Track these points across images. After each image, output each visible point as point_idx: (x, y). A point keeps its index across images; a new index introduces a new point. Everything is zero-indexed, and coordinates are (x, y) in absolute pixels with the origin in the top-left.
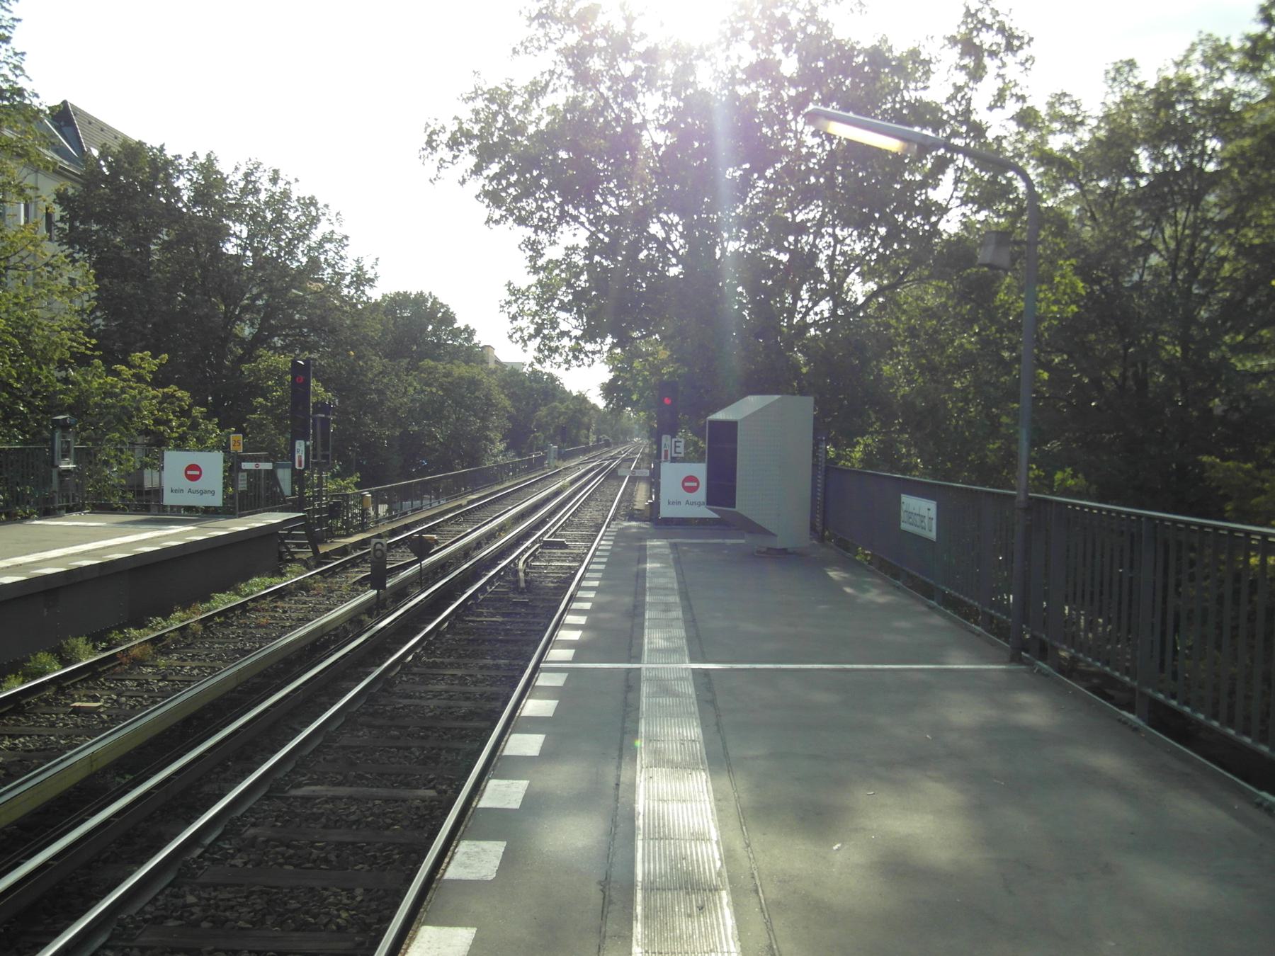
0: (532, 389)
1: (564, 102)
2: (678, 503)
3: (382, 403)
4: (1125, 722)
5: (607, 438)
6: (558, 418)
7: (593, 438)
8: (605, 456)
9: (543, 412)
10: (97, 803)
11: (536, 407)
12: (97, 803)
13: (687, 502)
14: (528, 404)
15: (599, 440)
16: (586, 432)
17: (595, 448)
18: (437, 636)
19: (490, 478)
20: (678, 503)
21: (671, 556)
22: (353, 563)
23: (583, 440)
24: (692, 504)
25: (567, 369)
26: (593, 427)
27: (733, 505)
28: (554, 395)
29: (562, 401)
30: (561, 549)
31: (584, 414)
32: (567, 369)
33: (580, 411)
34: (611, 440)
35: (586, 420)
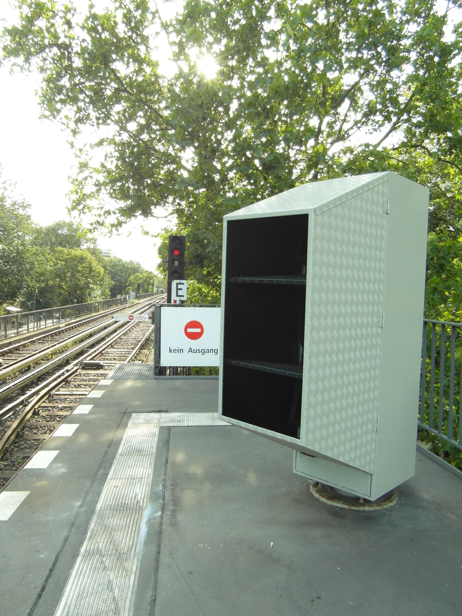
0: (128, 268)
1: (124, 25)
2: (181, 351)
3: (31, 269)
4: (448, 470)
5: (162, 289)
6: (139, 280)
7: (155, 290)
8: (159, 298)
9: (132, 277)
10: (105, 344)
11: (129, 276)
12: (105, 344)
13: (190, 350)
14: (126, 274)
15: (157, 291)
16: (151, 287)
17: (155, 294)
18: (50, 396)
19: (90, 309)
20: (181, 351)
21: (147, 513)
22: (151, 307)
23: (150, 290)
24: (195, 351)
25: (110, 237)
26: (155, 285)
27: (295, 432)
28: (138, 271)
29: (141, 273)
30: (95, 369)
31: (150, 279)
32: (110, 237)
33: (149, 277)
34: (164, 291)
35: (151, 281)
